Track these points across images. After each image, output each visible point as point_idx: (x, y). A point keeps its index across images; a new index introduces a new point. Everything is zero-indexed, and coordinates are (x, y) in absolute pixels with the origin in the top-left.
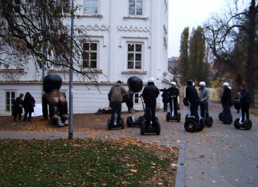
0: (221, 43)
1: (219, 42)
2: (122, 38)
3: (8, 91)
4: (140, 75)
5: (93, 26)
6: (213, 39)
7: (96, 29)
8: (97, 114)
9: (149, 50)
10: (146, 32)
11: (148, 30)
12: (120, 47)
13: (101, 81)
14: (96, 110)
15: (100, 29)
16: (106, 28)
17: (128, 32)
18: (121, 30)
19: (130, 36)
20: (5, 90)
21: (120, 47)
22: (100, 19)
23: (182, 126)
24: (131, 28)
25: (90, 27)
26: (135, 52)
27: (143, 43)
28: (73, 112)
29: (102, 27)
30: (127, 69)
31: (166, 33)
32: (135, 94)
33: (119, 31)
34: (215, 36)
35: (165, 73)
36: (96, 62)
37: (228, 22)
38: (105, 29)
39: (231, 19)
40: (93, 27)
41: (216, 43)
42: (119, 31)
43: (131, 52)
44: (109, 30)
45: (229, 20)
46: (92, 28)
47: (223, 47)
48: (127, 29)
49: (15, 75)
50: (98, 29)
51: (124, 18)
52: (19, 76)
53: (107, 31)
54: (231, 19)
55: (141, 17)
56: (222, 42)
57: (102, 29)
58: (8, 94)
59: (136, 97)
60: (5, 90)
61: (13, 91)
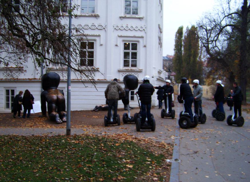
0: (214, 42)
1: (212, 41)
2: (118, 37)
3: (8, 89)
4: (136, 73)
5: (90, 25)
6: (206, 38)
7: (93, 28)
8: (94, 111)
9: (144, 48)
10: (141, 31)
11: (144, 29)
12: (116, 45)
13: (98, 79)
14: (93, 107)
15: (97, 28)
16: (103, 28)
17: (124, 31)
18: (117, 29)
19: (125, 35)
20: (5, 87)
21: (116, 45)
22: (97, 18)
23: (176, 123)
24: (127, 27)
25: (87, 26)
26: (130, 51)
27: (138, 42)
28: (71, 109)
29: (99, 27)
30: (123, 68)
31: (161, 32)
32: (131, 91)
33: (115, 30)
34: (209, 35)
35: (160, 71)
36: (93, 60)
37: (221, 22)
38: (102, 28)
39: (224, 18)
40: (90, 26)
41: (210, 42)
42: (115, 31)
43: (127, 51)
44: (106, 30)
45: (222, 19)
46: (89, 27)
47: (216, 46)
48: (123, 28)
49: (15, 73)
50: (95, 28)
51: (120, 17)
52: (18, 74)
53: (103, 31)
54: (224, 18)
55: (137, 16)
56: (215, 41)
57: (98, 28)
58: (8, 91)
59: (131, 95)
60: (5, 87)
61: (13, 89)
